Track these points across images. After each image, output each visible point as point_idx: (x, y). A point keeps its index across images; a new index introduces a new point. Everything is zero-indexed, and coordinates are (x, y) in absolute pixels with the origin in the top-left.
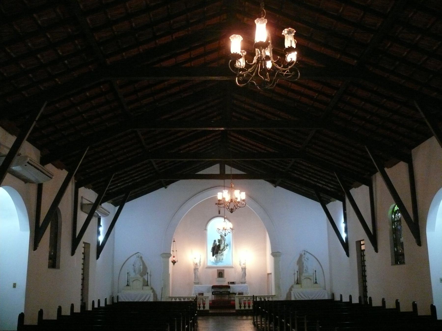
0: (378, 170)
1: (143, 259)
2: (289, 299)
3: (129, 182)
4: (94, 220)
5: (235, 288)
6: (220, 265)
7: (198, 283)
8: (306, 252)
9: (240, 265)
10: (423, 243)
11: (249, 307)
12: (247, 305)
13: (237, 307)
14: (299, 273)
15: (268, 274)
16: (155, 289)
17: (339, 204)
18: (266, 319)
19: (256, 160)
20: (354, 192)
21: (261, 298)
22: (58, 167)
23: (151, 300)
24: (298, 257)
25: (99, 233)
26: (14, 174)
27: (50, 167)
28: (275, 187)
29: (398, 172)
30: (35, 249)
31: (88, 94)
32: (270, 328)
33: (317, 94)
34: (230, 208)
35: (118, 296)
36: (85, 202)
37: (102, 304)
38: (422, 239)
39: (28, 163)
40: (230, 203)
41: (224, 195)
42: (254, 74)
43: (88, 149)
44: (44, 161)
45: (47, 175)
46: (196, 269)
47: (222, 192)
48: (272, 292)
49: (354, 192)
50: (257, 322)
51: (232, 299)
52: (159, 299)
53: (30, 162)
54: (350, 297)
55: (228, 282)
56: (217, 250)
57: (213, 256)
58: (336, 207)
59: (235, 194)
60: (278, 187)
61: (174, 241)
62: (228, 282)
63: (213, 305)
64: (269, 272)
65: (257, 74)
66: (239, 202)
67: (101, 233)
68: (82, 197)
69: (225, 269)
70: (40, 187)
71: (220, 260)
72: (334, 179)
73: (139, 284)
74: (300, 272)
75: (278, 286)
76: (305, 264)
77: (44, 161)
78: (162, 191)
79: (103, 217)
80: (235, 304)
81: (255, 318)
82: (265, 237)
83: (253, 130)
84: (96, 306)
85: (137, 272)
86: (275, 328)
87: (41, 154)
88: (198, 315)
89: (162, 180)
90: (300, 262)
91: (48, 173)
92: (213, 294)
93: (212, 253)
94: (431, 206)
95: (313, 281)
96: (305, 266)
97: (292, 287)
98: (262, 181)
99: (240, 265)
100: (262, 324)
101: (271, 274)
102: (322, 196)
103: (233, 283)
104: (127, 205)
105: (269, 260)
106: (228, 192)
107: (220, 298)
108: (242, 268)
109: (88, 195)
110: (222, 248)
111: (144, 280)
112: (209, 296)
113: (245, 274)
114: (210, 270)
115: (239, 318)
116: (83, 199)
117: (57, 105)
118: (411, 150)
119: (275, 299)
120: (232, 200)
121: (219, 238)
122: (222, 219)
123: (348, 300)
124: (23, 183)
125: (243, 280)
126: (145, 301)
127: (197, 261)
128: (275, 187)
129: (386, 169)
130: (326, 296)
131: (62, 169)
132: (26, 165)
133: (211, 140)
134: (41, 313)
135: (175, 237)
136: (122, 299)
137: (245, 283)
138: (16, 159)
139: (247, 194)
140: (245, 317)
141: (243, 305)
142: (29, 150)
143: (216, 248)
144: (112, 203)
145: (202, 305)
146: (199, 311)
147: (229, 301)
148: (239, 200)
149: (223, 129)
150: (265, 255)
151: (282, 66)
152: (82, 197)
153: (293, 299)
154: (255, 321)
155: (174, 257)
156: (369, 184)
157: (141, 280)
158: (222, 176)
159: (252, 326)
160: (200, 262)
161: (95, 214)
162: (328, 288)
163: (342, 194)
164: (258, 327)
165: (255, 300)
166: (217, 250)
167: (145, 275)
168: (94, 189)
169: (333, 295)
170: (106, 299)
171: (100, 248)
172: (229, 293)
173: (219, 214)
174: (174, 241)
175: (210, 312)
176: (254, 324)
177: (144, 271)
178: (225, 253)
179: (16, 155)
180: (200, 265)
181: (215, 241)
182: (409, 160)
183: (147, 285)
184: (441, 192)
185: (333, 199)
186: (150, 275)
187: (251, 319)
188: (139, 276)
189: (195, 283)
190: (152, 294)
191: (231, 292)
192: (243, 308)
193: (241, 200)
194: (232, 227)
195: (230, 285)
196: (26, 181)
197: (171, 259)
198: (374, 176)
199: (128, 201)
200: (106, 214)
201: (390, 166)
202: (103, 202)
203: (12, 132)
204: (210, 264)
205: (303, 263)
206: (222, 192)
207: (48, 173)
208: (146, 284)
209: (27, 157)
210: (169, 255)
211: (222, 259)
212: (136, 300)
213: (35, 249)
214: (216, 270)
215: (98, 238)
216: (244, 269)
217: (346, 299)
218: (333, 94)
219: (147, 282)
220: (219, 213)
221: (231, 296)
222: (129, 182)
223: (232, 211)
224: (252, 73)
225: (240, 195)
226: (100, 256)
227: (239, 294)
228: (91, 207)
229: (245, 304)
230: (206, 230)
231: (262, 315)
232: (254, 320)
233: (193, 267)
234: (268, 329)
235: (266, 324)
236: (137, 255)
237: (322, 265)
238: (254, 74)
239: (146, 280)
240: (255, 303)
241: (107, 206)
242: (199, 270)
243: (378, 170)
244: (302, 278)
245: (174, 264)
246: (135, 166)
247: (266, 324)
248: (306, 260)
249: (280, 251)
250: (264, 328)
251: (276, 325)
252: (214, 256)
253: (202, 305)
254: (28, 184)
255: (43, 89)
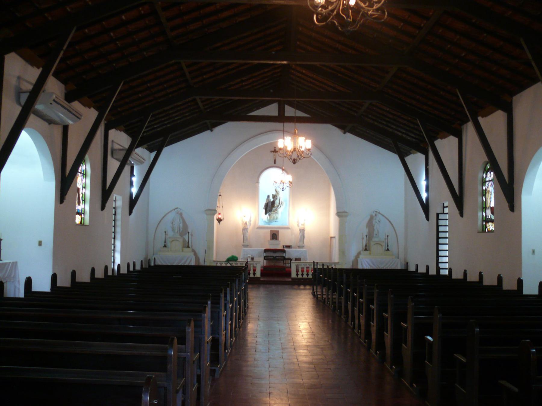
0: (470, 119)
1: (184, 216)
2: (354, 267)
3: (168, 124)
4: (127, 168)
5: (290, 253)
6: (274, 225)
7: (247, 246)
8: (377, 213)
9: (298, 225)
10: (516, 209)
11: (308, 275)
12: (305, 273)
13: (294, 275)
14: (369, 237)
15: (331, 238)
16: (197, 251)
17: (421, 157)
18: (329, 290)
19: (324, 100)
20: (439, 143)
21: (323, 265)
22: (84, 105)
23: (193, 264)
24: (369, 217)
25: (131, 184)
26: (40, 115)
27: (76, 105)
28: (345, 133)
29: (494, 123)
30: (62, 201)
31: (123, 17)
32: (332, 299)
33: (402, 24)
34: (293, 158)
35: (155, 259)
36: (116, 147)
37: (138, 267)
38: (516, 204)
39: (54, 100)
40: (292, 152)
41: (286, 143)
42: (335, 13)
43: (122, 84)
44: (70, 97)
45: (74, 114)
46: (245, 230)
47: (284, 139)
48: (336, 259)
49: (439, 143)
50: (317, 292)
51: (288, 265)
52: (202, 264)
53: (56, 100)
54: (427, 267)
55: (283, 246)
56: (270, 207)
57: (266, 214)
58: (416, 160)
59: (296, 141)
60: (348, 134)
61: (220, 195)
62: (283, 246)
63: (265, 271)
64: (332, 235)
65: (338, 13)
66: (303, 152)
67: (134, 184)
68: (113, 141)
69: (280, 231)
70: (65, 129)
71: (274, 219)
72: (416, 127)
73: (178, 245)
74: (370, 236)
75: (342, 252)
76: (376, 226)
77: (70, 97)
78: (206, 135)
79: (137, 165)
80: (291, 271)
81: (315, 287)
82: (329, 195)
83: (324, 66)
84: (131, 269)
85: (176, 231)
86: (339, 299)
87: (66, 89)
88: (249, 283)
89: (208, 121)
90: (370, 224)
91: (77, 112)
92: (265, 259)
93: (264, 211)
94: (531, 164)
95: (384, 248)
96: (376, 230)
97: (359, 253)
98: (329, 126)
99: (298, 225)
100: (323, 295)
101: (334, 237)
102: (401, 143)
103: (289, 247)
104: (166, 151)
105: (333, 221)
106: (292, 139)
107: (272, 264)
108: (300, 230)
109: (120, 139)
110: (277, 202)
111: (184, 241)
112: (260, 263)
113: (303, 236)
114: (262, 231)
115: (296, 287)
116: (114, 144)
117: (86, 30)
118: (512, 97)
119: (338, 267)
120: (295, 149)
121: (274, 193)
122: (279, 171)
123: (424, 271)
124: (46, 124)
125: (301, 244)
126: (186, 264)
127: (247, 220)
128: (345, 133)
129: (480, 119)
130: (399, 266)
131: (90, 108)
132: (51, 104)
133: (269, 74)
134: (74, 274)
135: (222, 191)
136: (158, 263)
137: (303, 247)
138: (42, 96)
139: (314, 144)
140: (302, 287)
141: (300, 273)
142: (54, 87)
143: (270, 204)
144: (146, 149)
145: (252, 272)
146: (251, 278)
147: (284, 268)
148: (303, 149)
149: (285, 62)
150: (328, 215)
151: (367, 4)
152: (113, 141)
153: (360, 267)
154: (315, 291)
155: (219, 214)
156: (459, 135)
157: (181, 240)
158: (281, 118)
159: (311, 296)
160: (250, 221)
161: (128, 162)
162: (402, 256)
163: (425, 146)
164: (317, 298)
165: (316, 267)
166: (270, 207)
167: (186, 234)
168: (126, 132)
169: (407, 264)
170: (142, 261)
171: (133, 202)
172: (284, 259)
173: (275, 164)
174: (220, 195)
175: (262, 279)
176: (314, 295)
177: (184, 230)
178: (280, 210)
179: (42, 91)
180: (250, 224)
181: (268, 196)
182: (508, 109)
183: (188, 247)
184: (541, 152)
185: (413, 150)
186: (192, 235)
187: (309, 289)
188: (178, 236)
189: (244, 246)
190: (194, 257)
191: (286, 257)
192: (300, 276)
193: (306, 149)
194: (291, 180)
195: (286, 249)
196: (50, 122)
197: (216, 217)
198: (465, 125)
199: (166, 146)
200: (140, 162)
201: (484, 116)
202: (137, 147)
203: (32, 62)
204: (261, 224)
205: (373, 226)
206: (284, 139)
207: (77, 112)
208: (187, 245)
209: (53, 93)
210: (214, 211)
211: (277, 218)
212: (181, 264)
213: (62, 201)
214: (269, 230)
215: (130, 190)
216: (302, 231)
217: (422, 270)
218: (422, 25)
219: (188, 243)
220: (275, 163)
221: (287, 261)
222: (168, 124)
223: (294, 162)
224: (332, 11)
225: (305, 143)
226: (134, 211)
227: (296, 260)
228: (124, 153)
229: (303, 271)
230: (258, 182)
231: (324, 284)
232: (313, 290)
233: (241, 227)
234: (331, 300)
235: (328, 295)
236: (176, 210)
237: (395, 226)
238: (335, 13)
239: (187, 240)
240: (315, 270)
241: (140, 151)
242: (249, 231)
243: (470, 119)
244: (372, 243)
245: (219, 223)
246: (176, 104)
247: (328, 295)
248: (377, 222)
249: (347, 211)
250: (325, 299)
251: (340, 295)
252: (268, 215)
253: (252, 272)
254: (52, 125)
255: (69, 10)
